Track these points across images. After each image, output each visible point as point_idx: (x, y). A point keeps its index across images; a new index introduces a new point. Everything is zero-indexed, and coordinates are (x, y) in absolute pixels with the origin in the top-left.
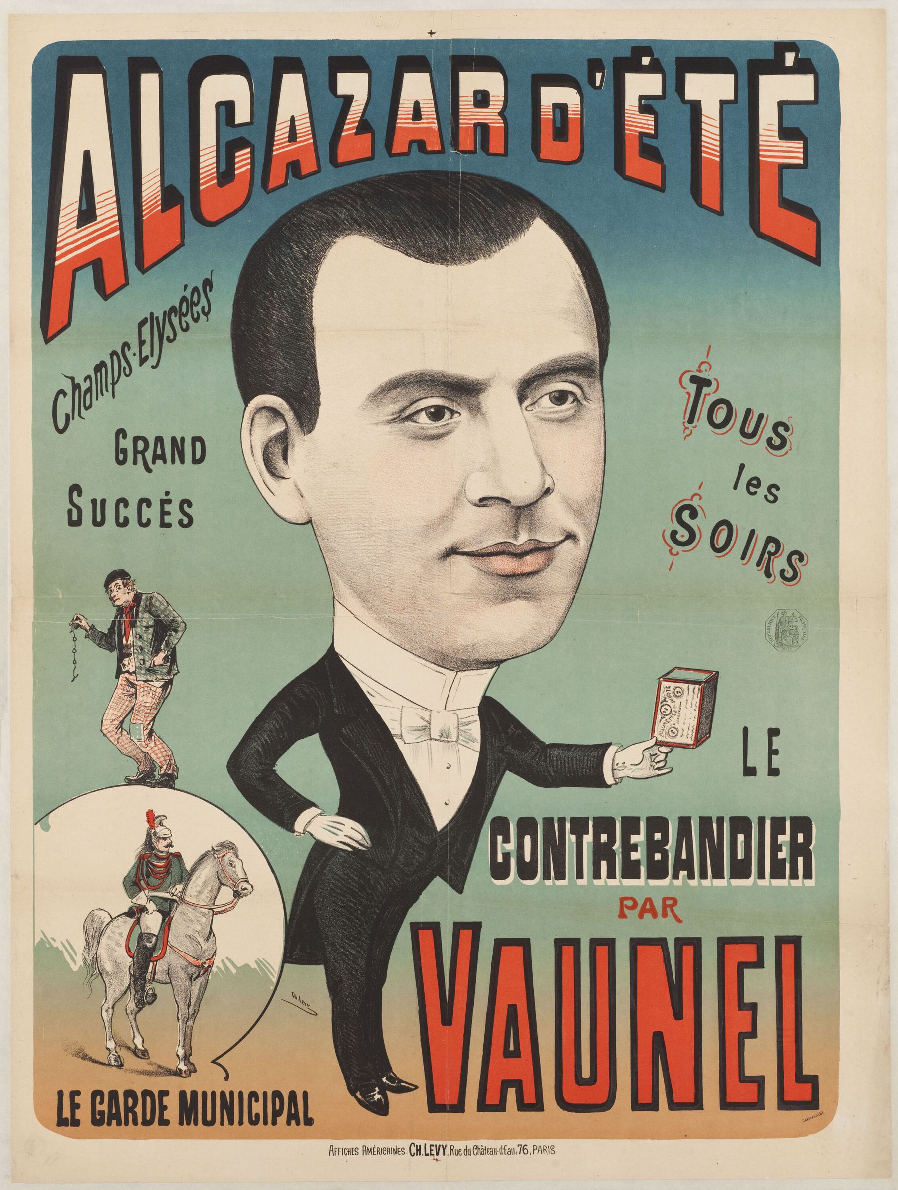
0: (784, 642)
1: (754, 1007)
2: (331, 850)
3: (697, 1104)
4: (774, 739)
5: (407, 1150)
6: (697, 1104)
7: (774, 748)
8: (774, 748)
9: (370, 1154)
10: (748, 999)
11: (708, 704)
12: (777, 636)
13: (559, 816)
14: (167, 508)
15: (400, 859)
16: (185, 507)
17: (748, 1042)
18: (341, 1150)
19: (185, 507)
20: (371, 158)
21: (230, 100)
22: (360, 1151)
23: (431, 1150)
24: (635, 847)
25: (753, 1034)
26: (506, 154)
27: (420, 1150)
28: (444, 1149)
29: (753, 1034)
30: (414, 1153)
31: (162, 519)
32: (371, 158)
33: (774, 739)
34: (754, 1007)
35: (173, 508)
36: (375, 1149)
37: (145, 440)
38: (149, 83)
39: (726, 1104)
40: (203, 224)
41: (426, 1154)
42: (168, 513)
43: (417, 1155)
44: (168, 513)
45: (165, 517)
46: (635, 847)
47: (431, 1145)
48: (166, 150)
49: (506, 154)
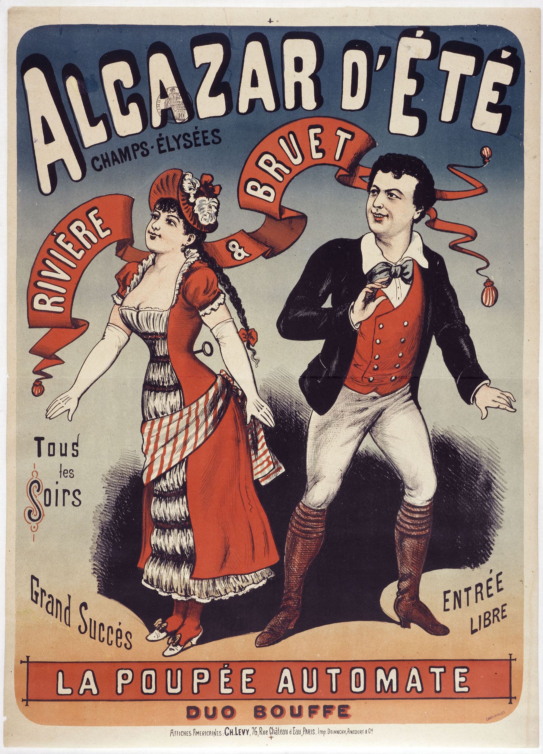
4: (415, 224)
5: (223, 732)
7: (446, 598)
8: (446, 598)
9: (198, 735)
14: (206, 135)
18: (178, 732)
22: (192, 732)
23: (240, 732)
24: (198, 138)
27: (232, 732)
28: (248, 732)
30: (228, 734)
31: (159, 149)
33: (415, 224)
35: (188, 733)
36: (201, 732)
37: (489, 612)
38: (52, 252)
41: (236, 734)
42: (207, 137)
44: (207, 137)
45: (197, 141)
47: (239, 730)
48: (27, 116)
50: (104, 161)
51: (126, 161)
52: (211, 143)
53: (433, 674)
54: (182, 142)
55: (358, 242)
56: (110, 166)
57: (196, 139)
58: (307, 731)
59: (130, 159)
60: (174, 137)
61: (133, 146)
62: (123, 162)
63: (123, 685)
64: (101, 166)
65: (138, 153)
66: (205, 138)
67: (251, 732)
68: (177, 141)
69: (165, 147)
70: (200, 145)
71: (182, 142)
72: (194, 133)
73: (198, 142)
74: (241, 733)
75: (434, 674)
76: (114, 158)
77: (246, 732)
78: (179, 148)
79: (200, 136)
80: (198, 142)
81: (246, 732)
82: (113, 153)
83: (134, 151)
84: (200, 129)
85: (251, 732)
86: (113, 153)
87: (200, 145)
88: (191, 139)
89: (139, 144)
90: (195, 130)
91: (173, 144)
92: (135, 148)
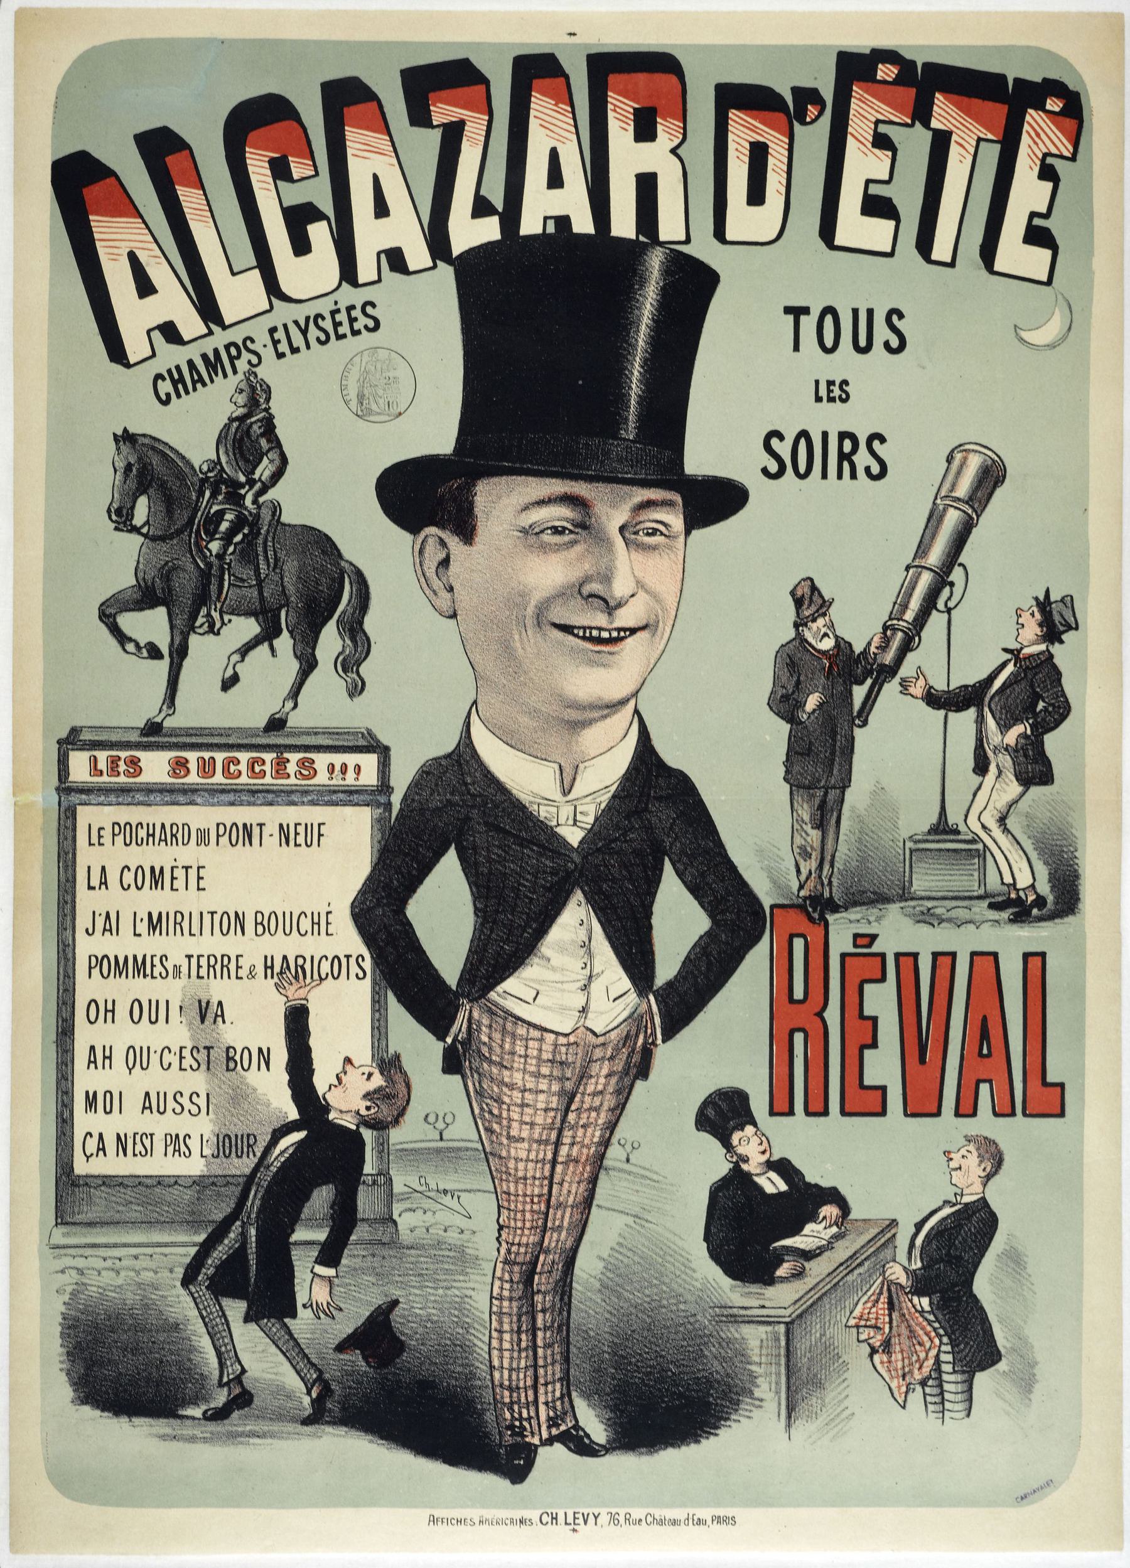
0: (374, 407)
1: (874, 1020)
2: (718, 917)
3: (825, 1113)
5: (536, 1519)
6: (825, 1113)
10: (867, 1012)
11: (67, 976)
12: (361, 398)
13: (404, 67)
15: (720, 1231)
16: (895, 318)
17: (868, 1054)
19: (895, 318)
20: (891, 254)
21: (714, 267)
23: (575, 1518)
24: (340, 324)
25: (874, 1045)
26: (952, 264)
28: (596, 1518)
29: (874, 1045)
32: (891, 254)
34: (874, 1020)
39: (844, 1113)
40: (367, 587)
43: (179, 396)
46: (340, 324)
49: (952, 264)
50: (175, 383)
51: (217, 375)
52: (363, 331)
53: (870, 1023)
54: (313, 333)
55: (466, 747)
56: (187, 392)
57: (337, 325)
58: (719, 1520)
59: (225, 376)
60: (296, 323)
61: (227, 347)
62: (212, 381)
63: (911, 851)
64: (168, 395)
65: (119, 839)
66: (352, 320)
67: (604, 1519)
68: (304, 332)
69: (283, 347)
70: (344, 336)
71: (313, 333)
72: (333, 313)
73: (341, 330)
74: (581, 1521)
75: (810, 1110)
76: (196, 377)
77: (591, 1517)
78: (308, 347)
79: (342, 317)
80: (341, 330)
81: (591, 1517)
82: (191, 364)
83: (232, 359)
84: (180, 864)
85: (604, 1519)
86: (191, 364)
87: (344, 336)
88: (328, 325)
89: (240, 344)
90: (334, 308)
91: (298, 340)
92: (233, 352)
